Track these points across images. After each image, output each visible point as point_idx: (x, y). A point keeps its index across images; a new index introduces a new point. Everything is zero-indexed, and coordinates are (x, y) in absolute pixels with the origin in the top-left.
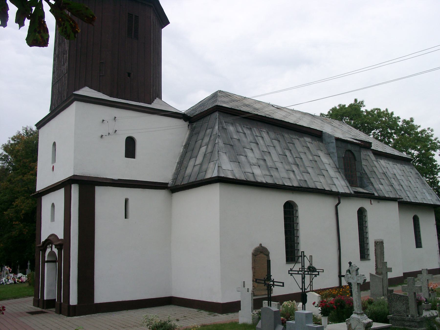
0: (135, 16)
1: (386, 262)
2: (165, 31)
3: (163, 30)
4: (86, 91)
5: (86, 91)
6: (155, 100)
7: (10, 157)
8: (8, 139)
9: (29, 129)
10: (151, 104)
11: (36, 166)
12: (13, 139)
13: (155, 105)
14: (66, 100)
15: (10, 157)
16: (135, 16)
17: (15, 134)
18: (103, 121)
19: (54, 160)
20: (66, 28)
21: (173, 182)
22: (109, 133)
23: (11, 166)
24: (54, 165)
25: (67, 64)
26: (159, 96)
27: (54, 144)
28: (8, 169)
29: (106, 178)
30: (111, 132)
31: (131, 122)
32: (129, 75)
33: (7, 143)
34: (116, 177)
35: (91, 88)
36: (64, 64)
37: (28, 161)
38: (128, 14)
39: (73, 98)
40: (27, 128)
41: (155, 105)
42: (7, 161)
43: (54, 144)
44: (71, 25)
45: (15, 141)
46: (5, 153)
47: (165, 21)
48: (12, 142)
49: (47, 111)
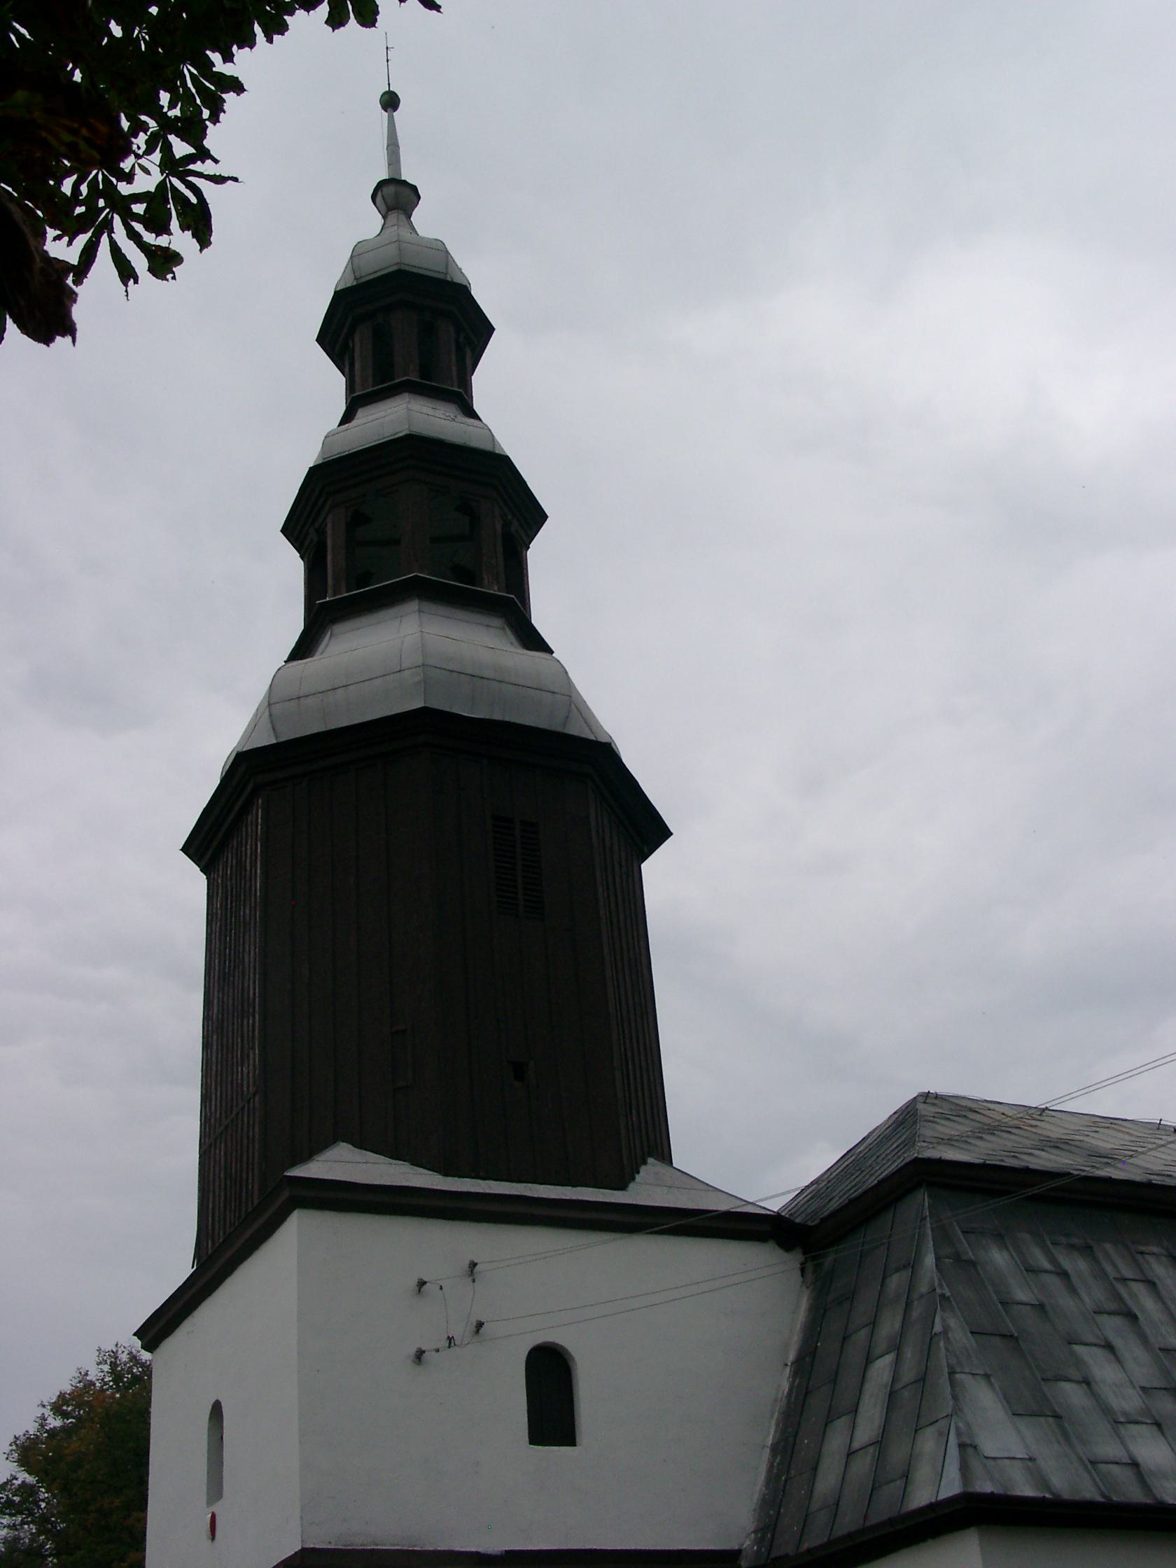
2: (656, 871)
4: (340, 1163)
5: (340, 1163)
6: (643, 1169)
7: (43, 1494)
9: (124, 1357)
10: (623, 1187)
11: (143, 1521)
12: (57, 1408)
13: (646, 1190)
15: (43, 1494)
17: (65, 1383)
18: (422, 1283)
19: (215, 1489)
21: (759, 1542)
22: (450, 1339)
23: (52, 1534)
24: (216, 1508)
27: (217, 1411)
28: (35, 1553)
30: (460, 1330)
31: (547, 1281)
32: (519, 1071)
33: (32, 1428)
35: (361, 1144)
39: (286, 1194)
40: (115, 1355)
41: (646, 1190)
42: (31, 1514)
43: (217, 1411)
45: (65, 1415)
46: (24, 1477)
47: (649, 830)
48: (55, 1422)
49: (179, 1266)
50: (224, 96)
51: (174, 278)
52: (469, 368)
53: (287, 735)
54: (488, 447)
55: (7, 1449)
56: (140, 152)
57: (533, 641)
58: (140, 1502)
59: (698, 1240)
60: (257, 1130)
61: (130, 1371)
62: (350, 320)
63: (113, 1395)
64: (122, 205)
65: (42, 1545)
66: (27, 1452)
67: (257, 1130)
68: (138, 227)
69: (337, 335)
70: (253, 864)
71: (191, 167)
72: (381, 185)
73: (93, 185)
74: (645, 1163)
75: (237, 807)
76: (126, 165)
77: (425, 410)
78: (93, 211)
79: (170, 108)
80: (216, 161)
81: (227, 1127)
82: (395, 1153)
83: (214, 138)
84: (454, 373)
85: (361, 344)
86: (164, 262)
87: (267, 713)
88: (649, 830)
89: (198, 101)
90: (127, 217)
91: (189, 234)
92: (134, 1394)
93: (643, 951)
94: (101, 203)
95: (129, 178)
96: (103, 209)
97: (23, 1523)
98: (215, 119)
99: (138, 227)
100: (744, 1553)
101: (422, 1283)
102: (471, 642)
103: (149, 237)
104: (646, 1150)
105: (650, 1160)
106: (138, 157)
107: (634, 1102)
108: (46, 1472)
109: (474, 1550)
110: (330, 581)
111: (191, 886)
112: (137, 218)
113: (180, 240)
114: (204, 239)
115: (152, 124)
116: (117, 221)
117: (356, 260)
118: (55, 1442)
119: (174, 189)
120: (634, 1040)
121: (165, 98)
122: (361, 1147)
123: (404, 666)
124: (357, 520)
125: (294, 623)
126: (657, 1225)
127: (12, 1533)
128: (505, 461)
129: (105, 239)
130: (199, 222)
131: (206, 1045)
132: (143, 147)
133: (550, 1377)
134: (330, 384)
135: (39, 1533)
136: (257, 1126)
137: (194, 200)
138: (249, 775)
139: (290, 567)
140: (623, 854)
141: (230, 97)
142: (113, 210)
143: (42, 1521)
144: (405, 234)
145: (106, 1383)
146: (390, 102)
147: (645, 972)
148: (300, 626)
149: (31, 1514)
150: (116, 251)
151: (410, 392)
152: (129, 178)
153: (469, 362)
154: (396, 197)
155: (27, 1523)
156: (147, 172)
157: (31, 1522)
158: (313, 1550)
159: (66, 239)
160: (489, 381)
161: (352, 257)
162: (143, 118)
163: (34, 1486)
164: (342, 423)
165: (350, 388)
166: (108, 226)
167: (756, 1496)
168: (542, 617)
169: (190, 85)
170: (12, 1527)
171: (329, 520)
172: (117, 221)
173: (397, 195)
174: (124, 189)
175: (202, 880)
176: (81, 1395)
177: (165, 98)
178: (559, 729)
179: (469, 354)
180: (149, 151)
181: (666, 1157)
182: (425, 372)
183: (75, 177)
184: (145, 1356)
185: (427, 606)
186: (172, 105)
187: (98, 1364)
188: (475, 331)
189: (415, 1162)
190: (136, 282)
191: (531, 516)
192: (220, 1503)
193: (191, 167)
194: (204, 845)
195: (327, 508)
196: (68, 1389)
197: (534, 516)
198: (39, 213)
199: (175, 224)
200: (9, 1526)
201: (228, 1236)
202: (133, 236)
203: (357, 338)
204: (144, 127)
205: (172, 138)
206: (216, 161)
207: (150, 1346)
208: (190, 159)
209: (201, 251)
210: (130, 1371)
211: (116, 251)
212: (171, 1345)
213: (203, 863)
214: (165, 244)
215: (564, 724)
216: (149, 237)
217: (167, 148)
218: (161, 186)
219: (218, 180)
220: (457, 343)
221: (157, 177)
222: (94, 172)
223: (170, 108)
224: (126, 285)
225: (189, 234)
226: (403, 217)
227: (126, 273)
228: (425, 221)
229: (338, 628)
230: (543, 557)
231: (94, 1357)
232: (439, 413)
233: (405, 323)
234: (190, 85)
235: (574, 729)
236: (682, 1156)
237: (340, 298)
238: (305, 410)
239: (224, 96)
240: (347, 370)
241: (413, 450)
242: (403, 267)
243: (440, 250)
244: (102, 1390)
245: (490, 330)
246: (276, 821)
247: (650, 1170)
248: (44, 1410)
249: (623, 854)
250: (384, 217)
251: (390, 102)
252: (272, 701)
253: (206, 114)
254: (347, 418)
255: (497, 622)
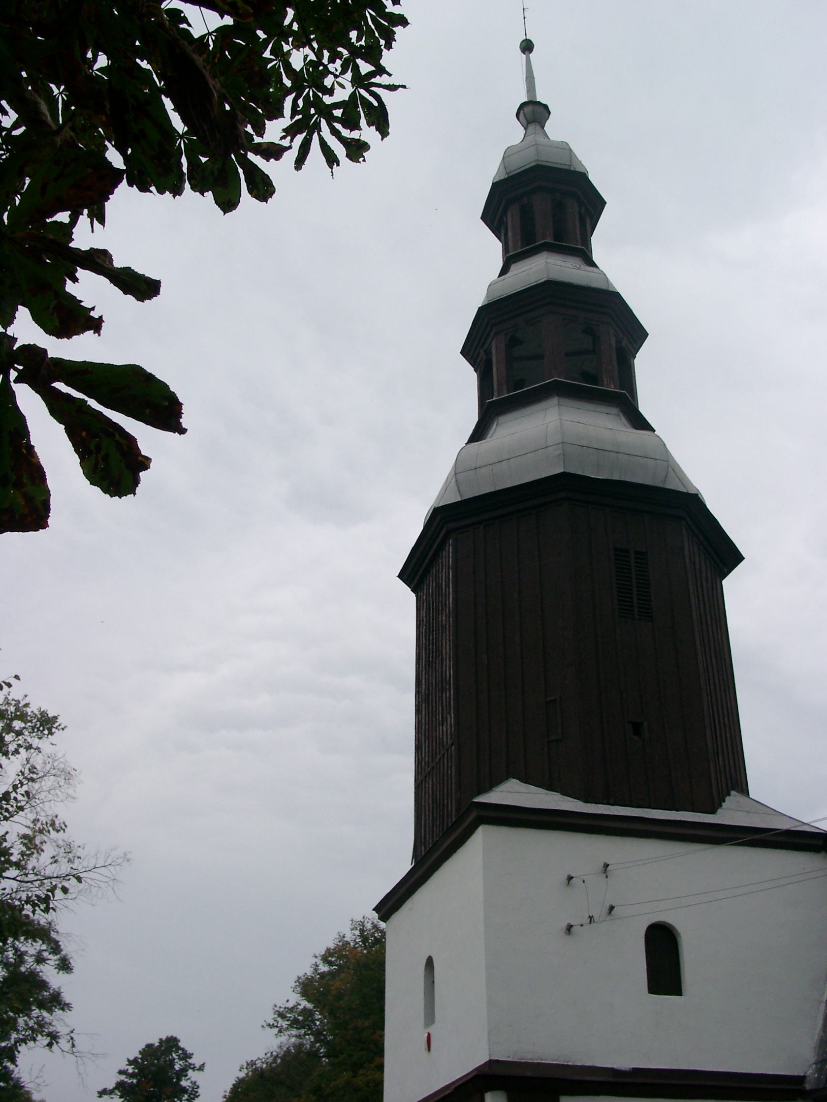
0: (636, 552)
1: (268, 161)
2: (734, 587)
3: (723, 582)
4: (512, 793)
5: (512, 793)
6: (727, 799)
7: (318, 1016)
8: (314, 960)
9: (369, 926)
10: (713, 812)
11: (382, 1036)
12: (325, 959)
13: (730, 813)
14: (455, 826)
15: (318, 1016)
16: (636, 552)
17: (331, 943)
18: (570, 878)
19: (430, 1017)
20: (106, 457)
21: (819, 1071)
22: (591, 918)
23: (325, 1043)
24: (431, 1030)
25: (451, 719)
26: (736, 779)
27: (430, 963)
28: (313, 1055)
29: (595, 1067)
30: (598, 911)
31: (658, 878)
32: (637, 728)
33: (309, 972)
34: (624, 1062)
35: (526, 780)
36: (444, 720)
37: (367, 1023)
38: (616, 549)
39: (474, 815)
40: (362, 924)
41: (730, 813)
42: (310, 1029)
43: (430, 963)
44: (118, 443)
45: (330, 963)
46: (305, 1004)
47: (728, 556)
48: (324, 968)
49: (403, 864)
50: (394, 29)
51: (364, 160)
52: (589, 234)
53: (469, 494)
54: (604, 287)
55: (294, 985)
56: (338, 73)
57: (640, 423)
58: (380, 1025)
59: (774, 850)
60: (453, 770)
61: (373, 935)
62: (504, 202)
63: (362, 953)
64: (326, 112)
65: (319, 1049)
66: (306, 987)
67: (453, 770)
68: (338, 126)
69: (493, 216)
70: (447, 585)
71: (373, 80)
72: (523, 106)
73: (306, 99)
74: (729, 795)
75: (435, 546)
76: (328, 81)
77: (558, 262)
78: (307, 117)
79: (357, 42)
80: (390, 75)
81: (433, 768)
82: (550, 786)
83: (387, 59)
84: (578, 236)
85: (512, 218)
86: (356, 150)
87: (454, 480)
88: (728, 556)
89: (377, 35)
90: (331, 119)
91: (373, 128)
92: (376, 951)
93: (725, 643)
94: (313, 111)
95: (330, 92)
96: (314, 115)
97: (305, 1034)
98: (389, 46)
99: (338, 126)
100: (808, 1079)
101: (570, 878)
102: (595, 425)
103: (346, 133)
104: (730, 785)
105: (733, 793)
106: (336, 76)
107: (720, 751)
108: (319, 1002)
109: (610, 1066)
110: (495, 387)
111: (406, 599)
112: (337, 120)
113: (367, 133)
114: (384, 131)
115: (345, 52)
116: (323, 123)
117: (506, 160)
118: (324, 982)
119: (362, 97)
120: (720, 707)
121: (353, 35)
122: (526, 782)
123: (549, 444)
124: (513, 342)
125: (472, 417)
126: (737, 839)
127: (299, 1041)
128: (617, 295)
129: (315, 137)
130: (380, 119)
131: (418, 711)
132: (340, 69)
133: (662, 944)
134: (492, 249)
135: (316, 1041)
136: (453, 767)
137: (376, 104)
138: (443, 523)
139: (469, 377)
140: (709, 574)
141: (398, 30)
142: (320, 116)
143: (318, 1034)
144: (541, 139)
145: (357, 943)
146: (527, 47)
147: (727, 657)
148: (476, 419)
149: (310, 1029)
150: (323, 144)
151: (548, 250)
152: (330, 92)
153: (588, 227)
154: (533, 113)
155: (308, 1035)
156: (343, 87)
157: (311, 1034)
158: (497, 1061)
159: (289, 138)
160: (604, 243)
161: (503, 158)
162: (340, 49)
163: (311, 1010)
164: (499, 276)
165: (506, 250)
166: (317, 127)
167: (816, 1037)
168: (645, 408)
169: (370, 23)
170: (298, 1036)
171: (493, 344)
172: (323, 123)
173: (533, 112)
174: (327, 100)
175: (413, 596)
176: (340, 951)
177: (353, 35)
178: (661, 485)
179: (588, 221)
180: (343, 72)
181: (744, 790)
182: (558, 236)
183: (294, 94)
184: (382, 925)
185: (564, 401)
186: (359, 39)
187: (352, 930)
188: (591, 204)
189: (564, 793)
190: (338, 165)
191: (634, 334)
192: (433, 1026)
193: (373, 80)
194: (414, 572)
195: (492, 334)
196: (332, 946)
197: (638, 335)
198: (260, 110)
199: (363, 122)
200: (296, 1036)
201: (436, 844)
202: (335, 133)
203: (509, 214)
204: (340, 55)
205: (359, 61)
206: (390, 75)
207: (384, 917)
208: (372, 75)
209: (382, 139)
210: (373, 935)
211: (323, 144)
212: (399, 917)
213: (413, 586)
214: (357, 137)
215: (664, 481)
216: (346, 133)
217: (356, 68)
218: (353, 96)
219: (392, 88)
220: (580, 213)
221: (350, 89)
222: (307, 90)
223: (357, 42)
224: (331, 168)
225: (373, 128)
226: (539, 127)
227: (331, 159)
228: (554, 129)
229: (502, 419)
230: (646, 364)
231: (349, 925)
232: (568, 265)
233: (545, 203)
234: (370, 23)
235: (672, 485)
236: (755, 790)
237: (496, 186)
238: (476, 266)
239: (394, 29)
240: (503, 238)
241: (550, 292)
242: (540, 163)
243: (565, 148)
244: (355, 948)
245: (603, 203)
246: (462, 555)
247: (733, 799)
248: (316, 960)
249: (709, 574)
250: (526, 129)
251: (527, 47)
252: (457, 472)
253: (382, 42)
254: (504, 271)
255: (615, 410)
